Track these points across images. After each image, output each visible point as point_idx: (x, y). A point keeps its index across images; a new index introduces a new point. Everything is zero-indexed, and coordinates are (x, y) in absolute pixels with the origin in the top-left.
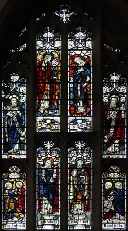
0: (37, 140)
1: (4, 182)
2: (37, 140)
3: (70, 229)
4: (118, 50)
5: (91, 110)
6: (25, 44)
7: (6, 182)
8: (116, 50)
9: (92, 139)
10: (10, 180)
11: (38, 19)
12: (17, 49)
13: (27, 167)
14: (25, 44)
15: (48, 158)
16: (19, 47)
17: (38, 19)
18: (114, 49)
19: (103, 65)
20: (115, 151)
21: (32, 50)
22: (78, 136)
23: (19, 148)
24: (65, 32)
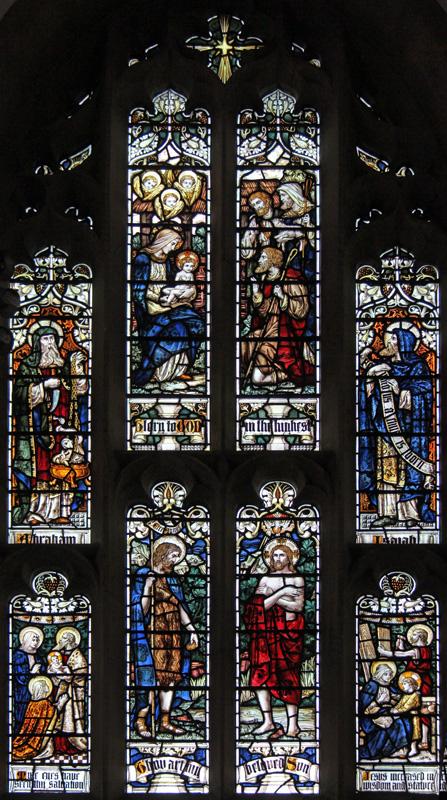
0: (121, 478)
1: (240, 756)
2: (121, 478)
3: (243, 790)
4: (407, 172)
5: (238, 306)
6: (90, 147)
7: (19, 627)
8: (402, 172)
9: (322, 478)
10: (33, 619)
11: (132, 62)
12: (63, 165)
13: (94, 572)
14: (90, 147)
15: (164, 541)
16: (66, 156)
17: (132, 62)
18: (394, 168)
19: (362, 222)
20: (393, 519)
21: (108, 172)
22: (277, 467)
23: (385, 716)
24: (224, 109)
